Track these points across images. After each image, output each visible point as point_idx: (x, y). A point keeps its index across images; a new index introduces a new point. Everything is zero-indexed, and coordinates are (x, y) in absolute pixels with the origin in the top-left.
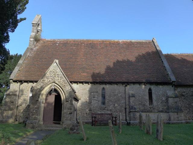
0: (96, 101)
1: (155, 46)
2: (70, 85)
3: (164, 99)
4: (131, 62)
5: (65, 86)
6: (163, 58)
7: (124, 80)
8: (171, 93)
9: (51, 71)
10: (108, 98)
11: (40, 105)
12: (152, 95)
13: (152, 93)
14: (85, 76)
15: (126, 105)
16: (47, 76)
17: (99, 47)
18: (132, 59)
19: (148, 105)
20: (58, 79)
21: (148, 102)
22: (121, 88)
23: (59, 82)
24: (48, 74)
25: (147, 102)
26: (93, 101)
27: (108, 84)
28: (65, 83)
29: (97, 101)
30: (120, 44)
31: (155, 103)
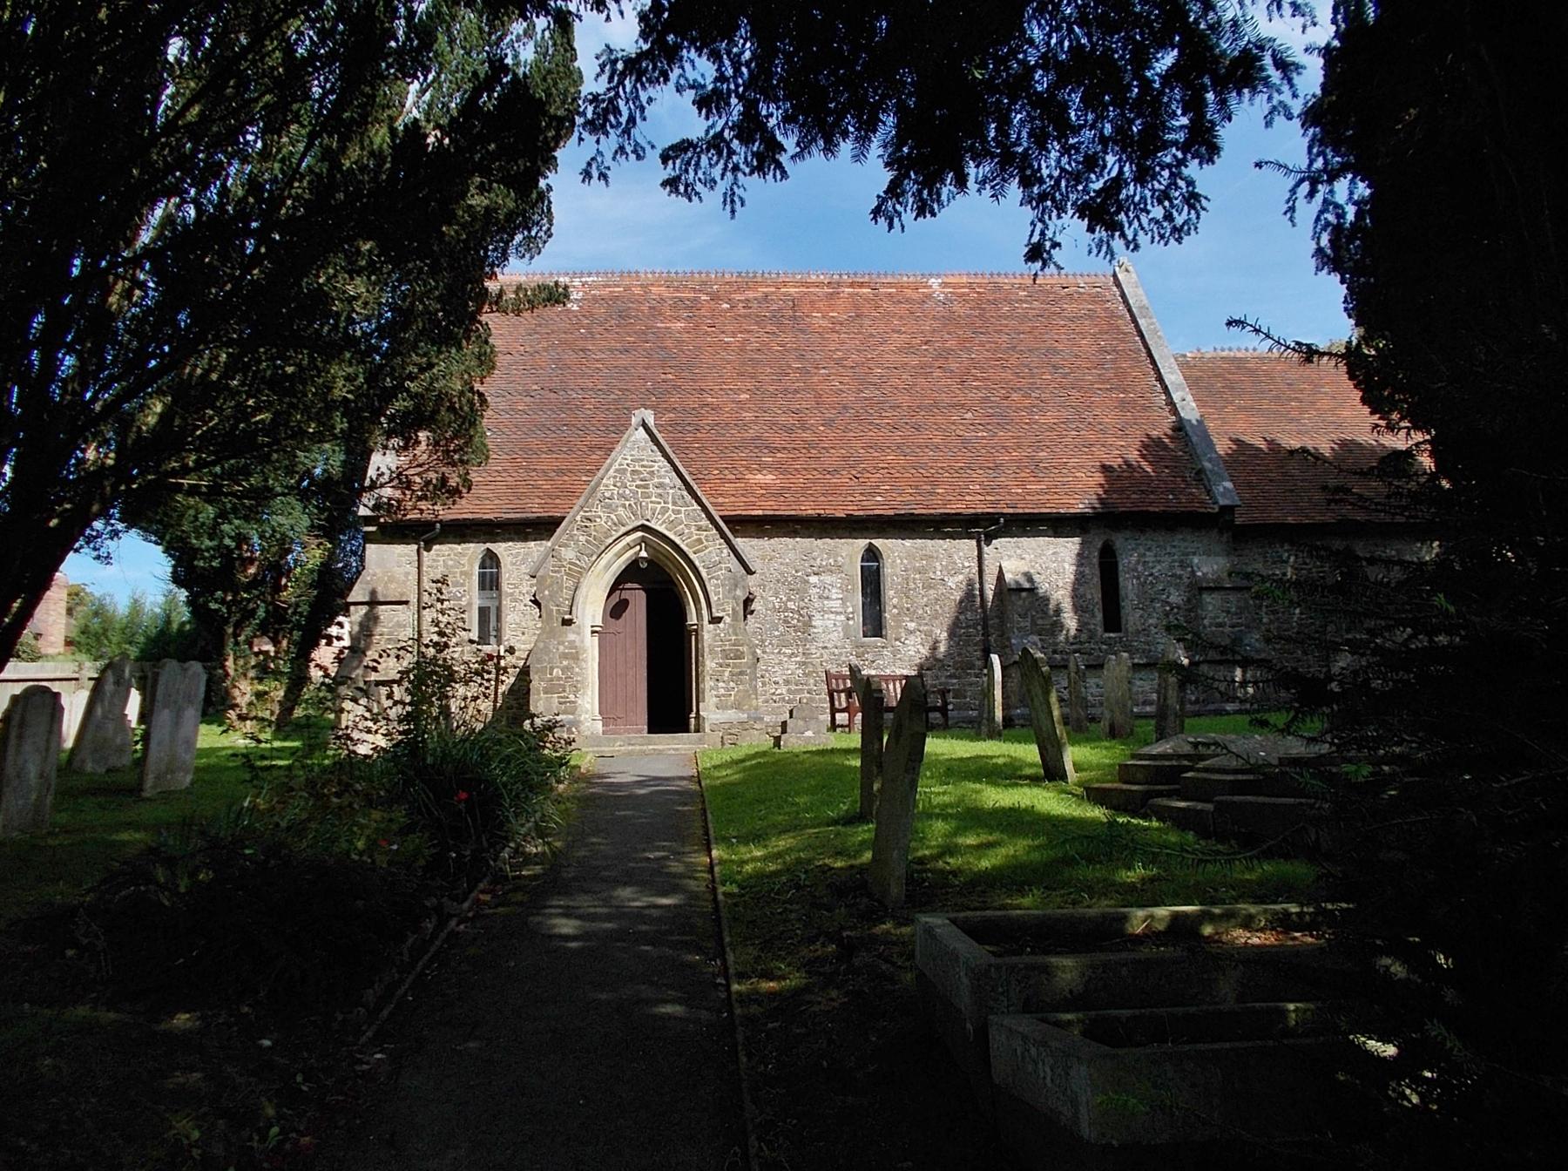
0: (832, 616)
1: (1130, 310)
2: (723, 535)
3: (1175, 598)
4: (1318, 457)
5: (699, 541)
6: (1173, 377)
7: (973, 502)
8: (1215, 567)
9: (626, 470)
10: (895, 601)
11: (582, 642)
12: (1117, 579)
13: (1121, 568)
14: (766, 487)
15: (986, 634)
16: (605, 498)
17: (817, 319)
18: (1325, 448)
19: (1100, 630)
20: (664, 510)
21: (1099, 616)
22: (965, 548)
23: (672, 524)
24: (608, 483)
25: (1093, 616)
26: (818, 616)
27: (840, 520)
28: (699, 529)
29: (838, 618)
30: (929, 296)
31: (1132, 617)
